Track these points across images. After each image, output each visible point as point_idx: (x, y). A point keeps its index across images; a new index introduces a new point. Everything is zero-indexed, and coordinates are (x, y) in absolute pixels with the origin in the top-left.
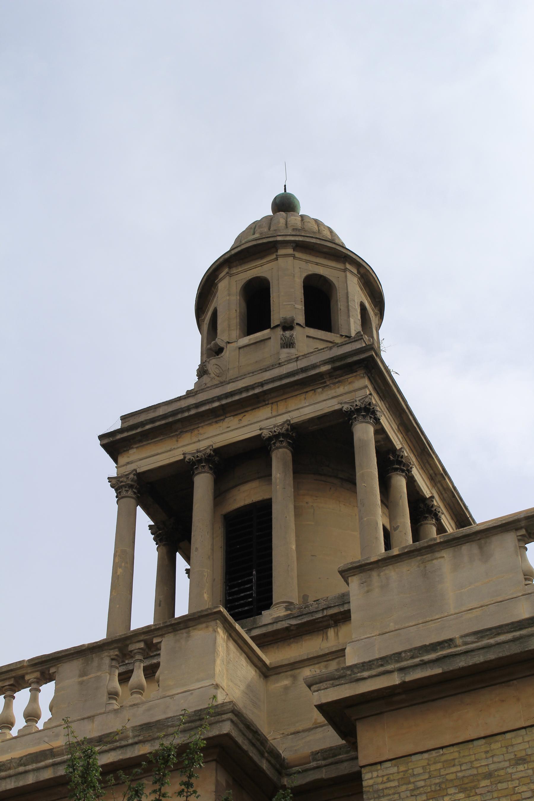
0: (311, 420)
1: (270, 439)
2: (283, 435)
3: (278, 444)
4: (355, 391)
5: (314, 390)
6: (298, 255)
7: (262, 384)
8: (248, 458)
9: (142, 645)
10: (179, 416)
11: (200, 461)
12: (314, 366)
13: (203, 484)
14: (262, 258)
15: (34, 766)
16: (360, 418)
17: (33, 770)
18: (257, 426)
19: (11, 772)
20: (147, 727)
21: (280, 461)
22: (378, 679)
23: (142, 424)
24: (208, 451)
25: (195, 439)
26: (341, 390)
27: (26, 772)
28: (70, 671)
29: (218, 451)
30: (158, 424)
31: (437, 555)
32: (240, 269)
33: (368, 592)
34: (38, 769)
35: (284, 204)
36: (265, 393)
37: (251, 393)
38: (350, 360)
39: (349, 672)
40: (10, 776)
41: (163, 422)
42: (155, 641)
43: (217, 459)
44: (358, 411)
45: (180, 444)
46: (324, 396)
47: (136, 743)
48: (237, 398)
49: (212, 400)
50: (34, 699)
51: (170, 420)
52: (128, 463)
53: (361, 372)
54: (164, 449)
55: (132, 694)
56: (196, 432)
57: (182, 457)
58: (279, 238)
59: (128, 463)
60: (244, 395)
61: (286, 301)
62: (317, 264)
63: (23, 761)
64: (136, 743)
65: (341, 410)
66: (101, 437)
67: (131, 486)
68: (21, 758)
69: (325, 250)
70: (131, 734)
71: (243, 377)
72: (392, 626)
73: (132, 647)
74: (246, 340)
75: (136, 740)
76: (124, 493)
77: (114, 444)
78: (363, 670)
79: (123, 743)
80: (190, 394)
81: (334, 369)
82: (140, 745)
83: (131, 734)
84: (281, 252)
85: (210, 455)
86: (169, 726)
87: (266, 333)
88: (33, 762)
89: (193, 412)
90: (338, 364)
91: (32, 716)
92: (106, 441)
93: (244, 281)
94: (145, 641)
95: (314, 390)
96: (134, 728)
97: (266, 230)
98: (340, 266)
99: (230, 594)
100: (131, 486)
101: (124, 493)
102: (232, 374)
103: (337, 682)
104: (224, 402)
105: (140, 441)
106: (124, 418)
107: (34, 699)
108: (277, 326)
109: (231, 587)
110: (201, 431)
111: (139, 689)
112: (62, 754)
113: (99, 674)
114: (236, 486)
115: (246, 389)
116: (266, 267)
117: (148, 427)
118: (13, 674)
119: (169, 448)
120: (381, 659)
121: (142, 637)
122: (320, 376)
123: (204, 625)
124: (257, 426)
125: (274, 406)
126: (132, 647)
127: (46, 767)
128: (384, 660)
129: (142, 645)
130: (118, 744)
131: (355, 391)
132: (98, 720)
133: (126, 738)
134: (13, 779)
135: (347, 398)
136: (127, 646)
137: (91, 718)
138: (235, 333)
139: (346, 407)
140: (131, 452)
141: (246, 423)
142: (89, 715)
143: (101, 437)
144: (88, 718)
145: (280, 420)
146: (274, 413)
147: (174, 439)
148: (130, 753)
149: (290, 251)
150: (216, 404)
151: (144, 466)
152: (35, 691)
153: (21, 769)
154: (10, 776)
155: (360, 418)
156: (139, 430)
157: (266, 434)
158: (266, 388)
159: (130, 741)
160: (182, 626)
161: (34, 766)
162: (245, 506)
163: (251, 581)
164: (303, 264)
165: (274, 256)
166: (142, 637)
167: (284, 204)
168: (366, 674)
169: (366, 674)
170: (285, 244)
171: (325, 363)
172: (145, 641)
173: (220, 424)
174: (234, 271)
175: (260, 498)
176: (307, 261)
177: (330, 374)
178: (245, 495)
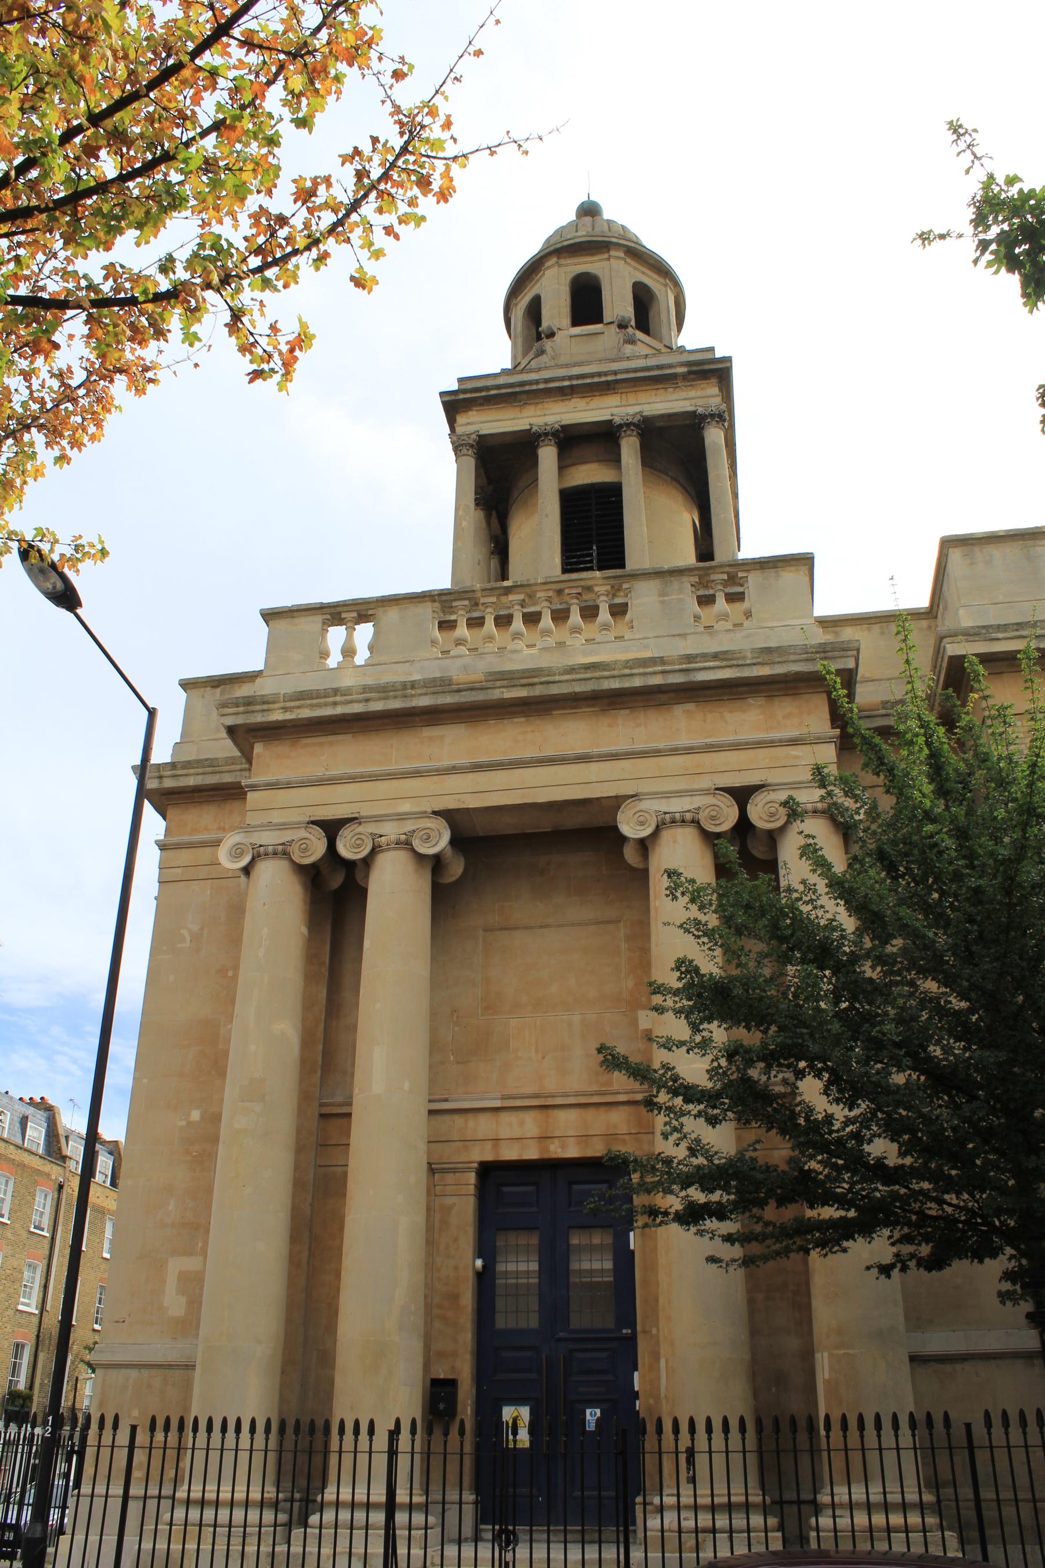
0: (662, 416)
1: (620, 426)
2: (634, 424)
3: (546, 442)
4: (709, 397)
5: (666, 389)
6: (628, 260)
7: (615, 373)
8: (602, 439)
9: (725, 577)
10: (527, 388)
11: (546, 434)
12: (670, 366)
13: (548, 456)
14: (592, 255)
15: (642, 670)
16: (714, 423)
17: (640, 674)
18: (608, 412)
19: (616, 673)
20: (768, 650)
21: (630, 449)
22: (677, 675)
23: (487, 388)
24: (556, 426)
25: (539, 413)
26: (692, 393)
27: (632, 675)
28: (392, 615)
29: (565, 428)
30: (503, 391)
31: (1039, 542)
32: (569, 261)
33: (972, 564)
34: (645, 674)
35: (589, 210)
36: (617, 381)
37: (603, 379)
38: (707, 367)
39: (984, 631)
40: (614, 677)
41: (509, 390)
42: (740, 575)
43: (562, 435)
44: (712, 416)
45: (524, 415)
46: (675, 396)
47: (754, 664)
48: (588, 381)
49: (563, 379)
50: (349, 637)
51: (517, 389)
52: (468, 424)
53: (714, 380)
54: (506, 417)
55: (513, 640)
56: (540, 406)
57: (528, 427)
58: (614, 240)
59: (468, 424)
60: (596, 380)
61: (618, 303)
62: (643, 273)
63: (628, 665)
64: (754, 664)
65: (695, 412)
66: (442, 394)
67: (472, 446)
68: (628, 661)
69: (652, 262)
70: (749, 655)
71: (589, 363)
72: (1001, 598)
73: (713, 577)
74: (578, 330)
75: (755, 661)
76: (464, 451)
77: (455, 405)
78: (998, 632)
79: (741, 662)
80: (505, 372)
81: (690, 373)
82: (759, 667)
83: (749, 655)
84: (613, 253)
85: (558, 431)
86: (790, 654)
87: (598, 327)
88: (640, 666)
89: (541, 386)
90: (695, 368)
91: (348, 651)
92: (447, 398)
93: (573, 275)
94: (728, 573)
95: (666, 389)
96: (753, 650)
97: (590, 229)
98: (662, 280)
99: (567, 564)
100: (472, 446)
101: (464, 451)
102: (563, 360)
103: (971, 638)
104: (575, 382)
105: (482, 405)
106: (461, 380)
107: (349, 637)
108: (612, 323)
109: (567, 558)
110: (546, 406)
111: (546, 633)
112: (674, 664)
113: (681, 596)
114: (574, 464)
115: (599, 374)
116: (597, 265)
117: (493, 392)
118: (582, 583)
119: (512, 416)
120: (1017, 624)
121: (727, 569)
122: (675, 376)
123: (793, 568)
124: (608, 412)
125: (624, 396)
126: (713, 577)
127: (655, 673)
128: (1020, 625)
129: (725, 577)
130: (735, 662)
131: (709, 397)
132: (690, 639)
133: (744, 658)
134: (617, 680)
135: (700, 402)
136: (709, 575)
137: (683, 636)
138: (566, 321)
139: (700, 410)
140: (470, 413)
141: (595, 407)
142: (681, 632)
143: (442, 394)
144: (679, 635)
145: (632, 410)
146: (624, 403)
147: (518, 409)
148: (747, 673)
149: (622, 255)
150: (567, 383)
151: (488, 429)
152: (351, 630)
153: (627, 671)
154: (614, 677)
155: (714, 423)
156: (484, 394)
157: (617, 420)
158: (619, 377)
159: (748, 662)
160: (771, 565)
161: (642, 670)
162: (583, 485)
163: (591, 555)
164: (631, 270)
165: (606, 256)
166: (727, 569)
167: (589, 210)
168: (1000, 635)
169: (1000, 635)
170: (618, 245)
171: (682, 364)
172: (728, 573)
173: (567, 403)
174: (562, 261)
175: (600, 480)
176: (635, 268)
177: (685, 377)
178: (589, 474)
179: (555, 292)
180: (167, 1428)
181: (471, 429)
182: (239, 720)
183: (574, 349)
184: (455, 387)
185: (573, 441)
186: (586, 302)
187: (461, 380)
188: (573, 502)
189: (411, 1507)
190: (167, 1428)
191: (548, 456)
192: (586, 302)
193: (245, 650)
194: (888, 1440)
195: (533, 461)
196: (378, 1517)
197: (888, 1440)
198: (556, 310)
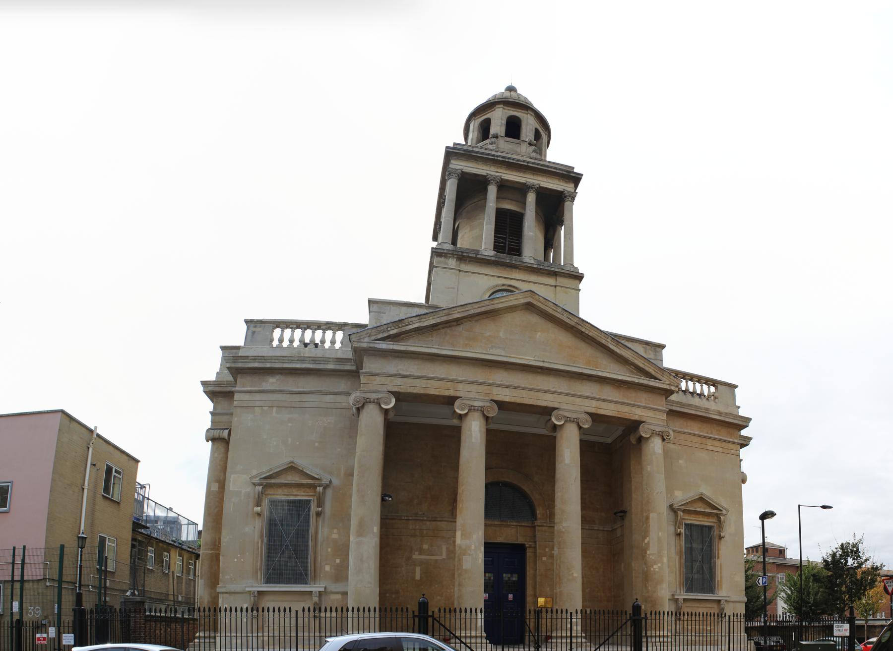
13: (492, 190)
21: (531, 198)
50: (292, 335)
106: (455, 144)
107: (292, 335)
152: (293, 332)
179: (498, 120)
180: (331, 611)
181: (458, 167)
182: (233, 365)
183: (505, 147)
184: (452, 145)
185: (504, 187)
186: (513, 128)
187: (455, 144)
188: (501, 215)
189: (577, 637)
190: (331, 611)
191: (492, 190)
192: (513, 128)
193: (238, 338)
194: (697, 618)
195: (485, 190)
196: (569, 641)
197: (697, 618)
198: (498, 127)
